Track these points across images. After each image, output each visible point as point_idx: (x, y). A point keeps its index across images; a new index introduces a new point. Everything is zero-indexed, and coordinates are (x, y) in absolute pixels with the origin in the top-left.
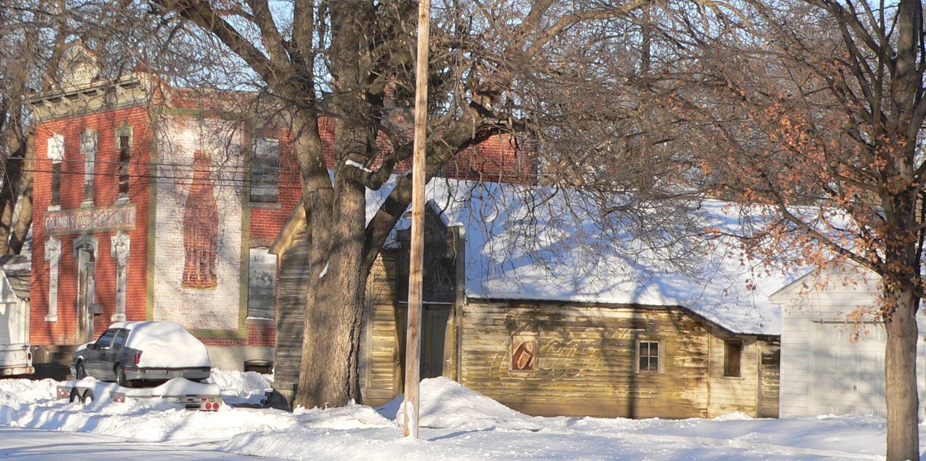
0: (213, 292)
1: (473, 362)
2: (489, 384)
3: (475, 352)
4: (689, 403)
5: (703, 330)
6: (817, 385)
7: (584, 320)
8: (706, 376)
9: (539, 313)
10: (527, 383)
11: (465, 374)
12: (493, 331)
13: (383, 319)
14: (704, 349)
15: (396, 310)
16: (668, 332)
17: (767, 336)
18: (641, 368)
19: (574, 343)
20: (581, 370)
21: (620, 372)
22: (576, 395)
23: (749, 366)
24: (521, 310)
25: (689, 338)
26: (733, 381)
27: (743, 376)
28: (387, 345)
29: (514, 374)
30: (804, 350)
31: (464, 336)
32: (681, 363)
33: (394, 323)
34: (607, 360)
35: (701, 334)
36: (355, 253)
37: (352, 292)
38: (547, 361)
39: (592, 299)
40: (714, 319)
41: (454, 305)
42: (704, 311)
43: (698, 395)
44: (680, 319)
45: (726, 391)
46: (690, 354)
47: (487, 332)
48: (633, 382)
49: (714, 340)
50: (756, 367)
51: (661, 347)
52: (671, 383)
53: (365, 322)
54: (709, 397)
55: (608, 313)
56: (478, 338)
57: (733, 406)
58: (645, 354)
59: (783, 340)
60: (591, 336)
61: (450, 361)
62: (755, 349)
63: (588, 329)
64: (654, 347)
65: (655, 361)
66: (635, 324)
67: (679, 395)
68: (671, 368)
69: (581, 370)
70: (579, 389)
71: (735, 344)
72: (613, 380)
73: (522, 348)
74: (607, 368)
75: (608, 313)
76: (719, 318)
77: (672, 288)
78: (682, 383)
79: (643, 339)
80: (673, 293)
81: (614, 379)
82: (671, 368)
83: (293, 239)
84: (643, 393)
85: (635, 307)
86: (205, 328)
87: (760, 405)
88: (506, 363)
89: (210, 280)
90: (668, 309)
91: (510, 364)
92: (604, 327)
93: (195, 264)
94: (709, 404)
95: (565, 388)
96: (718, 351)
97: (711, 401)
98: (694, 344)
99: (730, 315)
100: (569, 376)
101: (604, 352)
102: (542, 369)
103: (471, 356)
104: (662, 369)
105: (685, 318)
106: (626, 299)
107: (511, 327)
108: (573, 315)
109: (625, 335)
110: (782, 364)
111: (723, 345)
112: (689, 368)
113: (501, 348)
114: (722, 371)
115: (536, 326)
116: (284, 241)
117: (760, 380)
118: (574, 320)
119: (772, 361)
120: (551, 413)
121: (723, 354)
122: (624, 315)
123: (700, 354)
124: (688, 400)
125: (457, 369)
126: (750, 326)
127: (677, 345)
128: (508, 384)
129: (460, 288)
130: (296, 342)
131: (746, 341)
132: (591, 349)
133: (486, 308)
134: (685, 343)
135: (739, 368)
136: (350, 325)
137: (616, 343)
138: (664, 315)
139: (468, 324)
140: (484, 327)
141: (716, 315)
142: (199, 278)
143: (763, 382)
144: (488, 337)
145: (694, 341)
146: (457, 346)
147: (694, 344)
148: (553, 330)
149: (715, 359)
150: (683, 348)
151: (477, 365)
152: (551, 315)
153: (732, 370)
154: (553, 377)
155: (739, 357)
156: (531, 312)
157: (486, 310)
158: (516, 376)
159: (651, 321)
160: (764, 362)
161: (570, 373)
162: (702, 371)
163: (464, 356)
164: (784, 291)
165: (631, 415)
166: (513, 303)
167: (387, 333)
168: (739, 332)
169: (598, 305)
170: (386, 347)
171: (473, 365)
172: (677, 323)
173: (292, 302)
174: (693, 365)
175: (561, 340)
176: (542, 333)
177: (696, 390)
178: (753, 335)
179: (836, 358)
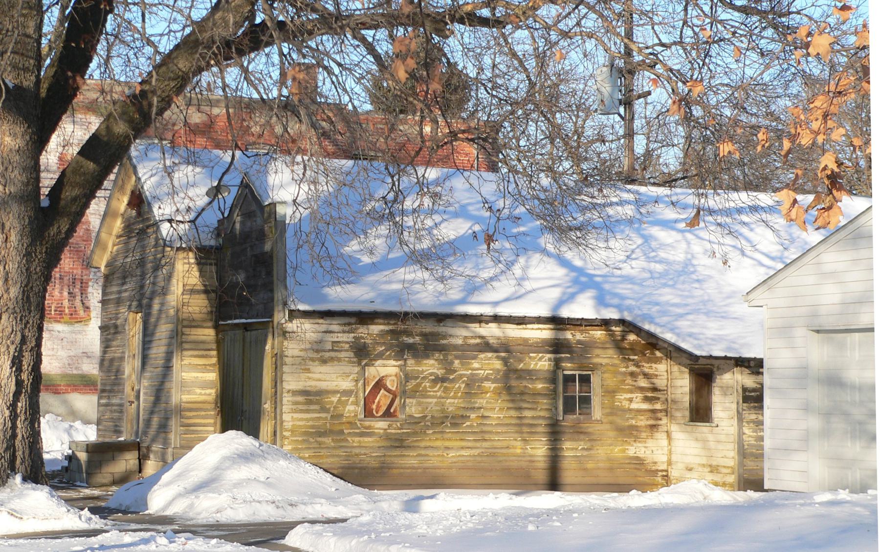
0: (86, 328)
1: (300, 407)
2: (328, 441)
3: (305, 393)
4: (639, 462)
5: (658, 354)
6: (826, 434)
7: (478, 341)
8: (664, 421)
9: (408, 334)
10: (387, 437)
11: (288, 425)
12: (332, 359)
13: (198, 345)
14: (661, 383)
15: (217, 335)
16: (606, 357)
17: (749, 360)
18: (566, 412)
19: (461, 376)
20: (473, 416)
21: (533, 418)
22: (463, 453)
23: (724, 406)
24: (376, 329)
25: (638, 366)
26: (703, 428)
27: (716, 421)
28: (205, 385)
29: (367, 424)
30: (802, 376)
31: (286, 369)
32: (626, 404)
33: (214, 353)
34: (513, 401)
35: (657, 360)
36: (16, 224)
37: (14, 291)
38: (419, 404)
39: (487, 311)
40: (669, 337)
41: (272, 322)
42: (656, 324)
43: (653, 450)
44: (624, 338)
45: (693, 444)
46: (642, 389)
47: (324, 361)
48: (555, 433)
49: (676, 368)
50: (734, 406)
51: (595, 380)
52: (612, 434)
53: (172, 353)
54: (670, 452)
55: (513, 332)
56: (308, 371)
57: (704, 465)
58: (570, 394)
59: (766, 364)
60: (488, 365)
61: (267, 406)
62: (733, 380)
63: (482, 356)
64: (585, 380)
65: (586, 401)
66: (557, 347)
67: (624, 451)
68: (614, 411)
69: (473, 416)
70: (470, 444)
71: (704, 372)
72: (522, 427)
73: (380, 385)
74: (513, 413)
75: (513, 332)
76: (678, 335)
77: (616, 295)
78: (630, 433)
79: (569, 368)
80: (615, 301)
81: (525, 429)
82: (614, 411)
83: (114, 245)
84: (570, 448)
85: (556, 322)
86: (75, 372)
87: (741, 464)
88: (353, 409)
89: (82, 313)
90: (605, 323)
91: (360, 409)
92: (507, 351)
93: (61, 293)
94: (669, 463)
95: (447, 444)
96: (682, 384)
97: (674, 458)
98: (646, 376)
99: (694, 330)
100: (454, 425)
101: (508, 389)
102: (411, 416)
103: (300, 399)
104: (597, 412)
105: (632, 337)
106: (544, 311)
107: (362, 353)
108: (459, 334)
109: (542, 363)
110: (767, 401)
111: (687, 376)
112: (639, 411)
113: (346, 384)
114: (687, 413)
115: (402, 351)
116: (105, 249)
117: (740, 426)
118: (460, 342)
119: (753, 398)
120: (435, 481)
121: (687, 389)
122: (544, 333)
123: (655, 389)
124: (637, 458)
125: (275, 418)
126: (723, 345)
127: (620, 378)
128: (357, 439)
129: (278, 295)
130: (114, 384)
131: (718, 368)
132: (487, 385)
133: (324, 324)
134: (633, 375)
135: (711, 409)
136: (12, 349)
137: (529, 374)
138: (599, 334)
139: (292, 349)
140: (321, 353)
141: (672, 330)
142: (67, 311)
143: (746, 430)
144: (324, 369)
145: (646, 370)
146: (276, 382)
147: (646, 376)
148: (427, 357)
149: (678, 397)
150: (629, 380)
151: (307, 411)
152: (424, 335)
153: (700, 413)
154: (428, 428)
155: (710, 393)
156: (392, 332)
157: (324, 328)
158: (369, 427)
159: (579, 342)
160: (746, 399)
161: (456, 420)
162: (659, 415)
163: (287, 399)
164: (765, 287)
165: (554, 485)
166: (364, 317)
167: (204, 368)
168: (704, 354)
169: (497, 319)
170: (202, 388)
171: (302, 411)
172: (619, 345)
173: (112, 331)
174: (645, 406)
175: (440, 373)
176: (411, 362)
177: (650, 443)
178: (726, 358)
179: (853, 387)
